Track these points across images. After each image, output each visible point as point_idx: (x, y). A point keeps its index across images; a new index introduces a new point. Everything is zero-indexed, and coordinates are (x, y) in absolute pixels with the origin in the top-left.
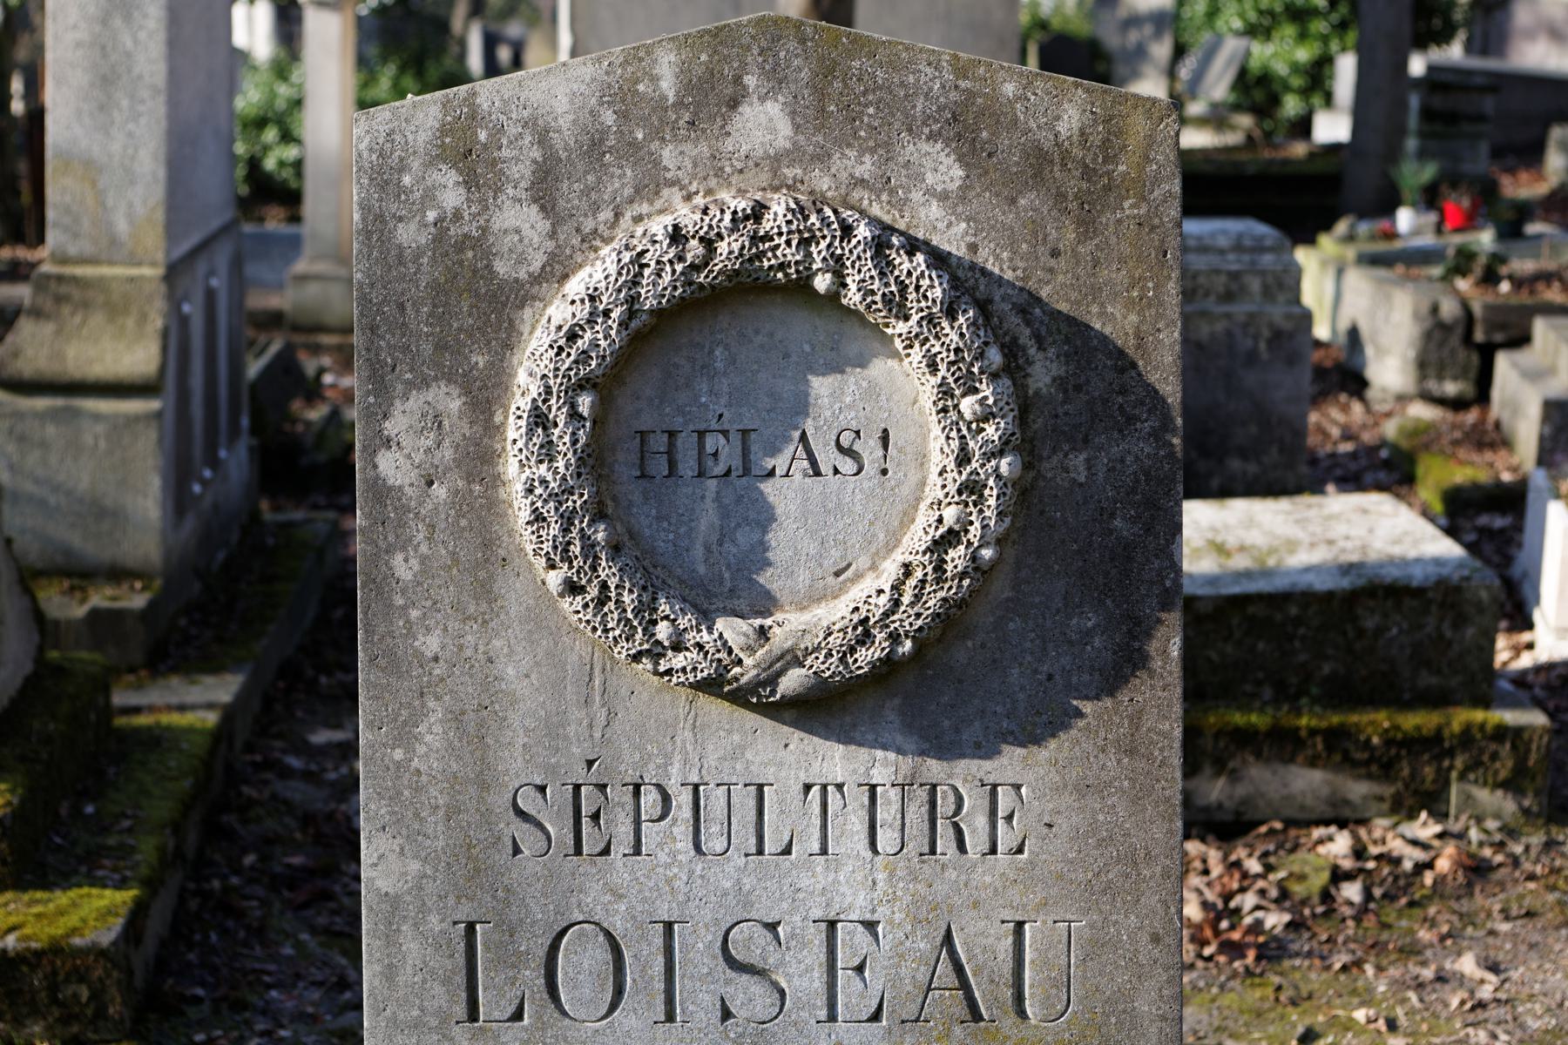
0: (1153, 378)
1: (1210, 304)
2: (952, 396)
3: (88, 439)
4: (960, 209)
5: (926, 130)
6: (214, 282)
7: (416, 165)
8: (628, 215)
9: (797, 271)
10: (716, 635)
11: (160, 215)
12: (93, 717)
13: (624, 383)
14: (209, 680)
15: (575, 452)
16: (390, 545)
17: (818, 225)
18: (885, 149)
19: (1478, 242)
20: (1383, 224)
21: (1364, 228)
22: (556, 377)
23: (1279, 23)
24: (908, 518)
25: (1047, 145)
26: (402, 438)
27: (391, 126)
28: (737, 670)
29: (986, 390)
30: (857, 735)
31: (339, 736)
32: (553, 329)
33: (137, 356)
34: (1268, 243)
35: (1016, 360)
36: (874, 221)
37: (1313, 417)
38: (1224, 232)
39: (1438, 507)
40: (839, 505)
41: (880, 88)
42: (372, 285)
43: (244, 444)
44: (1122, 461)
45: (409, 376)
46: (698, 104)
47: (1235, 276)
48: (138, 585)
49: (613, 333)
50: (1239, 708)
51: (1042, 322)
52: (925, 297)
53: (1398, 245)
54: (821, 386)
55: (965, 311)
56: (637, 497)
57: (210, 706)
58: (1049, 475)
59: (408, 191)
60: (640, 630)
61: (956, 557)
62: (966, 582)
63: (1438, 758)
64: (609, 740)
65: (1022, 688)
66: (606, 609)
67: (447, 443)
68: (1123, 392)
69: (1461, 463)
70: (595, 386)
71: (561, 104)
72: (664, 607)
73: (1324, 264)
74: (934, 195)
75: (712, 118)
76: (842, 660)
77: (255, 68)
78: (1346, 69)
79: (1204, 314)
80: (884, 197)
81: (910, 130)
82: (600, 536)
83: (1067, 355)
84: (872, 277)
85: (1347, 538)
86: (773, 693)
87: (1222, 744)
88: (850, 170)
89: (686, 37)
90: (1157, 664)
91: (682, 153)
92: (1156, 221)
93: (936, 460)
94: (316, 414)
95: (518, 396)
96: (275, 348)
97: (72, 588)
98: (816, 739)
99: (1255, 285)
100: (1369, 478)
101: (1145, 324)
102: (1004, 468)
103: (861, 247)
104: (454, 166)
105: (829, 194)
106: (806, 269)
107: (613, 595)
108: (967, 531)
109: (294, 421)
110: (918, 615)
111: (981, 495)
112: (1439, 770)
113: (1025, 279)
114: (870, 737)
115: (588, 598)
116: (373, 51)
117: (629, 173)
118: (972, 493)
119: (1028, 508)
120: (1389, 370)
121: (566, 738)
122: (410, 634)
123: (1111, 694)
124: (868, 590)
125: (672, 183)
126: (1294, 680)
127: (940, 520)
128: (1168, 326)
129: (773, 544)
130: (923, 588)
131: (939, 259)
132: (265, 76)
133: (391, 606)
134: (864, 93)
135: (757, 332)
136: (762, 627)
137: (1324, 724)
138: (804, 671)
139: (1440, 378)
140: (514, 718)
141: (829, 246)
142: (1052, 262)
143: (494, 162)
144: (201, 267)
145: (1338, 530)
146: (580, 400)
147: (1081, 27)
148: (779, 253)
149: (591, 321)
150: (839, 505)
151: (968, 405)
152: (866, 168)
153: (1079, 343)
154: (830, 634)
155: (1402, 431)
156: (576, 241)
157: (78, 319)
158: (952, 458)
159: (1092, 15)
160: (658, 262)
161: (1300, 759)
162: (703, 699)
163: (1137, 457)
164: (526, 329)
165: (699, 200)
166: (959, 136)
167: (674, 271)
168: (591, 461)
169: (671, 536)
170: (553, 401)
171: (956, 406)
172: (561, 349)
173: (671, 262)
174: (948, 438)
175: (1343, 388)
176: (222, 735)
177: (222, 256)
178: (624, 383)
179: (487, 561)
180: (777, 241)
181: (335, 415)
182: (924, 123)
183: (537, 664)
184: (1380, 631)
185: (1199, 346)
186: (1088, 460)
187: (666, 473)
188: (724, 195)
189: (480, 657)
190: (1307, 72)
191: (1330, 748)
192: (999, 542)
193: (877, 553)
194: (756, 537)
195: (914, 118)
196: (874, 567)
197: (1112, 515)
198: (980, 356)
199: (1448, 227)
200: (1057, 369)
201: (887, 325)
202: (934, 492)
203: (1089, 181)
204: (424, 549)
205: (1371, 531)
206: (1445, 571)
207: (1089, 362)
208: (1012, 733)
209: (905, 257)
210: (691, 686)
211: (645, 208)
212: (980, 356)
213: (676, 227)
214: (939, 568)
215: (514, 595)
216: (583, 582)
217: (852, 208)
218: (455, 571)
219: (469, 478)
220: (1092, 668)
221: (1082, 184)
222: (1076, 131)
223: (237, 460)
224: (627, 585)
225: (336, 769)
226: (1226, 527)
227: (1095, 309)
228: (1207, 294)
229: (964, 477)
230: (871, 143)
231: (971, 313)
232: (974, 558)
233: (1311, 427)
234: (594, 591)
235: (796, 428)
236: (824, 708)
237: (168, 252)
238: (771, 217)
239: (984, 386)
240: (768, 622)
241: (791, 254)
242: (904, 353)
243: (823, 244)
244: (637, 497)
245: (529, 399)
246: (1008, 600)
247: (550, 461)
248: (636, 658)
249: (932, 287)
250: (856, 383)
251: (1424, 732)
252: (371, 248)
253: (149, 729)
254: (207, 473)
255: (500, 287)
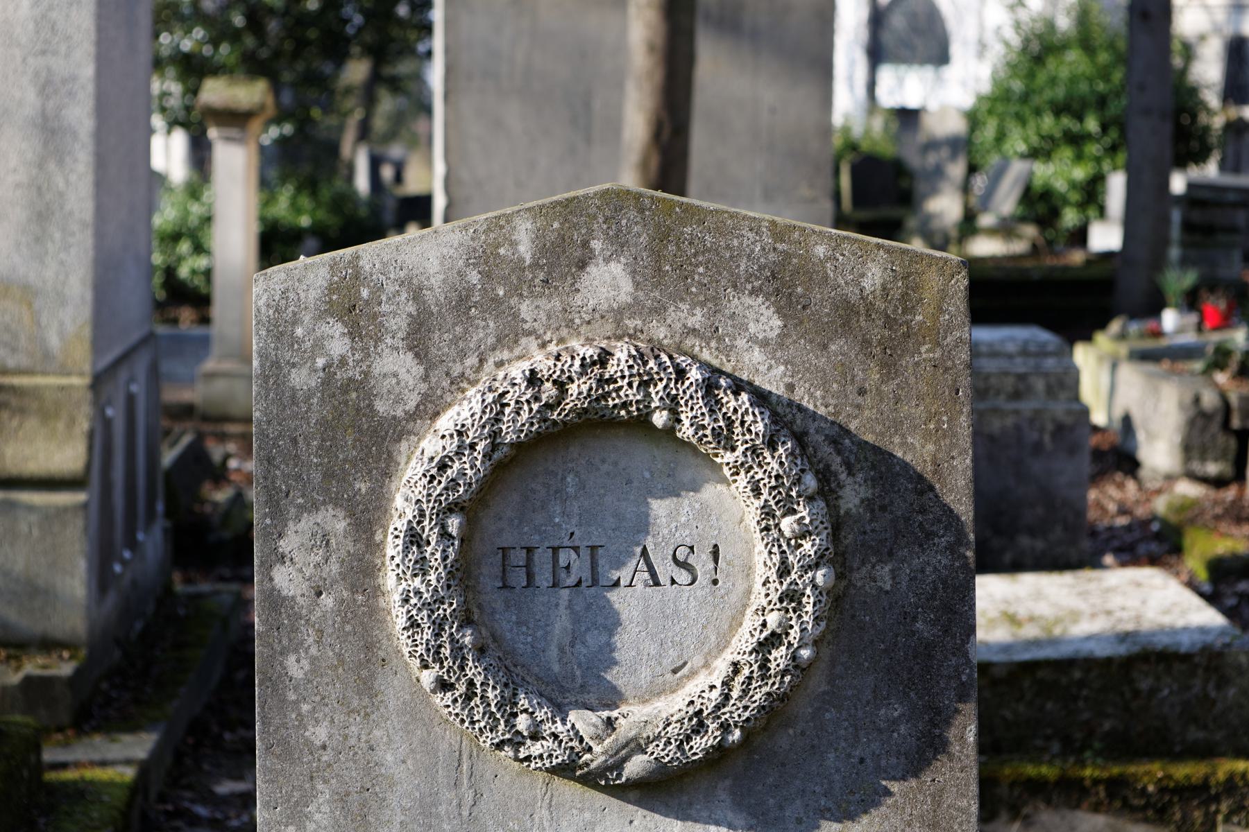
0: (949, 499)
1: (1001, 402)
2: (774, 517)
3: (23, 527)
4: (779, 354)
5: (749, 287)
6: (134, 388)
7: (307, 318)
8: (491, 361)
9: (638, 409)
10: (569, 726)
11: (87, 332)
12: (25, 773)
13: (488, 506)
14: (127, 738)
15: (445, 567)
16: (284, 648)
17: (656, 369)
18: (713, 303)
19: (1233, 340)
20: (1149, 324)
21: (1134, 327)
22: (429, 501)
23: (1058, 146)
24: (736, 623)
25: (854, 299)
26: (295, 554)
27: (285, 285)
28: (587, 756)
29: (803, 511)
30: (693, 812)
31: (240, 787)
32: (426, 460)
33: (67, 455)
34: (1051, 348)
35: (829, 484)
36: (704, 365)
37: (1093, 495)
38: (1012, 339)
39: (1202, 575)
40: (676, 611)
41: (709, 250)
42: (269, 422)
43: (160, 525)
44: (923, 571)
45: (300, 501)
46: (551, 265)
47: (1022, 377)
48: (66, 654)
49: (478, 463)
50: (1031, 761)
51: (851, 451)
52: (749, 431)
53: (1164, 343)
54: (659, 508)
55: (784, 443)
56: (499, 605)
57: (128, 762)
58: (859, 584)
59: (300, 341)
60: (502, 722)
61: (779, 657)
62: (787, 679)
63: (1206, 803)
64: (476, 818)
65: (838, 770)
66: (472, 704)
67: (333, 559)
68: (923, 511)
69: (1223, 535)
70: (462, 509)
71: (433, 266)
72: (523, 702)
73: (1100, 359)
74: (756, 343)
75: (563, 277)
76: (680, 747)
77: (170, 190)
78: (1116, 187)
79: (996, 411)
80: (713, 344)
81: (735, 287)
82: (467, 640)
83: (873, 479)
84: (703, 414)
85: (1123, 609)
86: (619, 776)
87: (1016, 793)
88: (683, 321)
89: (541, 207)
90: (955, 748)
91: (537, 307)
92: (949, 363)
93: (760, 573)
94: (222, 496)
95: (395, 518)
96: (186, 440)
97: (9, 658)
98: (657, 816)
99: (1039, 385)
100: (1142, 549)
101: (942, 454)
102: (820, 579)
103: (693, 388)
104: (340, 319)
105: (665, 342)
106: (646, 407)
107: (479, 691)
108: (787, 634)
109: (203, 502)
110: (746, 708)
111: (800, 603)
112: (1207, 814)
113: (836, 414)
114: (705, 814)
115: (457, 694)
116: (273, 174)
117: (492, 324)
118: (792, 601)
119: (841, 613)
120: (1159, 452)
121: (438, 816)
122: (302, 725)
123: (916, 775)
124: (702, 686)
125: (529, 333)
126: (1078, 735)
127: (764, 625)
128: (960, 454)
129: (619, 645)
130: (750, 684)
131: (761, 398)
132: (180, 196)
133: (284, 701)
134: (695, 255)
135: (603, 461)
136: (609, 718)
137: (1105, 775)
138: (646, 757)
139: (1203, 459)
140: (393, 799)
141: (665, 387)
142: (860, 400)
143: (375, 316)
144: (123, 375)
145: (1116, 601)
146: (450, 521)
147: (887, 149)
148: (622, 393)
149: (459, 454)
150: (676, 611)
151: (787, 524)
152: (697, 319)
153: (883, 469)
154: (668, 725)
155: (1170, 507)
156: (446, 383)
157: (15, 423)
158: (774, 570)
159: (897, 139)
160: (517, 402)
161: (1085, 805)
162: (558, 781)
163: (935, 568)
164: (403, 460)
165: (553, 348)
166: (777, 292)
167: (531, 410)
168: (459, 575)
169: (529, 639)
170: (426, 523)
171: (777, 525)
172: (433, 477)
173: (528, 402)
174: (770, 553)
175: (1119, 467)
176: (138, 788)
177: (141, 365)
178: (488, 506)
179: (368, 661)
180: (620, 384)
181: (239, 501)
182: (747, 281)
183: (412, 751)
184: (1153, 691)
185: (992, 439)
186: (892, 571)
187: (525, 584)
188: (574, 343)
189: (363, 745)
190: (1083, 189)
191: (1111, 796)
192: (816, 643)
193: (709, 653)
194: (603, 639)
195: (738, 276)
196: (706, 665)
197: (915, 619)
198: (798, 481)
199: (1207, 325)
200: (865, 492)
201: (716, 455)
202: (759, 600)
203: (890, 329)
204: (314, 651)
205: (1144, 602)
206: (1209, 639)
207: (892, 486)
208: (829, 810)
209: (731, 397)
210: (547, 770)
211: (505, 355)
212: (798, 481)
213: (532, 372)
214: (764, 666)
215: (392, 691)
216: (453, 680)
217: (685, 354)
218: (340, 670)
219: (354, 589)
220: (899, 752)
221: (884, 332)
222: (878, 287)
223: (153, 541)
224: (491, 682)
225: (238, 816)
226: (1018, 599)
227: (897, 440)
228: (998, 393)
229: (784, 587)
230: (702, 298)
231: (789, 445)
232: (794, 658)
233: (1090, 503)
234: (462, 688)
235: (638, 544)
236: (661, 789)
237: (94, 363)
238: (615, 362)
239: (801, 508)
240: (615, 714)
241: (633, 395)
242: (731, 479)
243: (660, 386)
244: (499, 605)
245: (405, 521)
246: (824, 693)
247: (424, 574)
248: (499, 746)
249: (755, 422)
250: (690, 505)
251: (1193, 780)
252: (268, 390)
253: (75, 783)
254: (127, 554)
255: (380, 424)
